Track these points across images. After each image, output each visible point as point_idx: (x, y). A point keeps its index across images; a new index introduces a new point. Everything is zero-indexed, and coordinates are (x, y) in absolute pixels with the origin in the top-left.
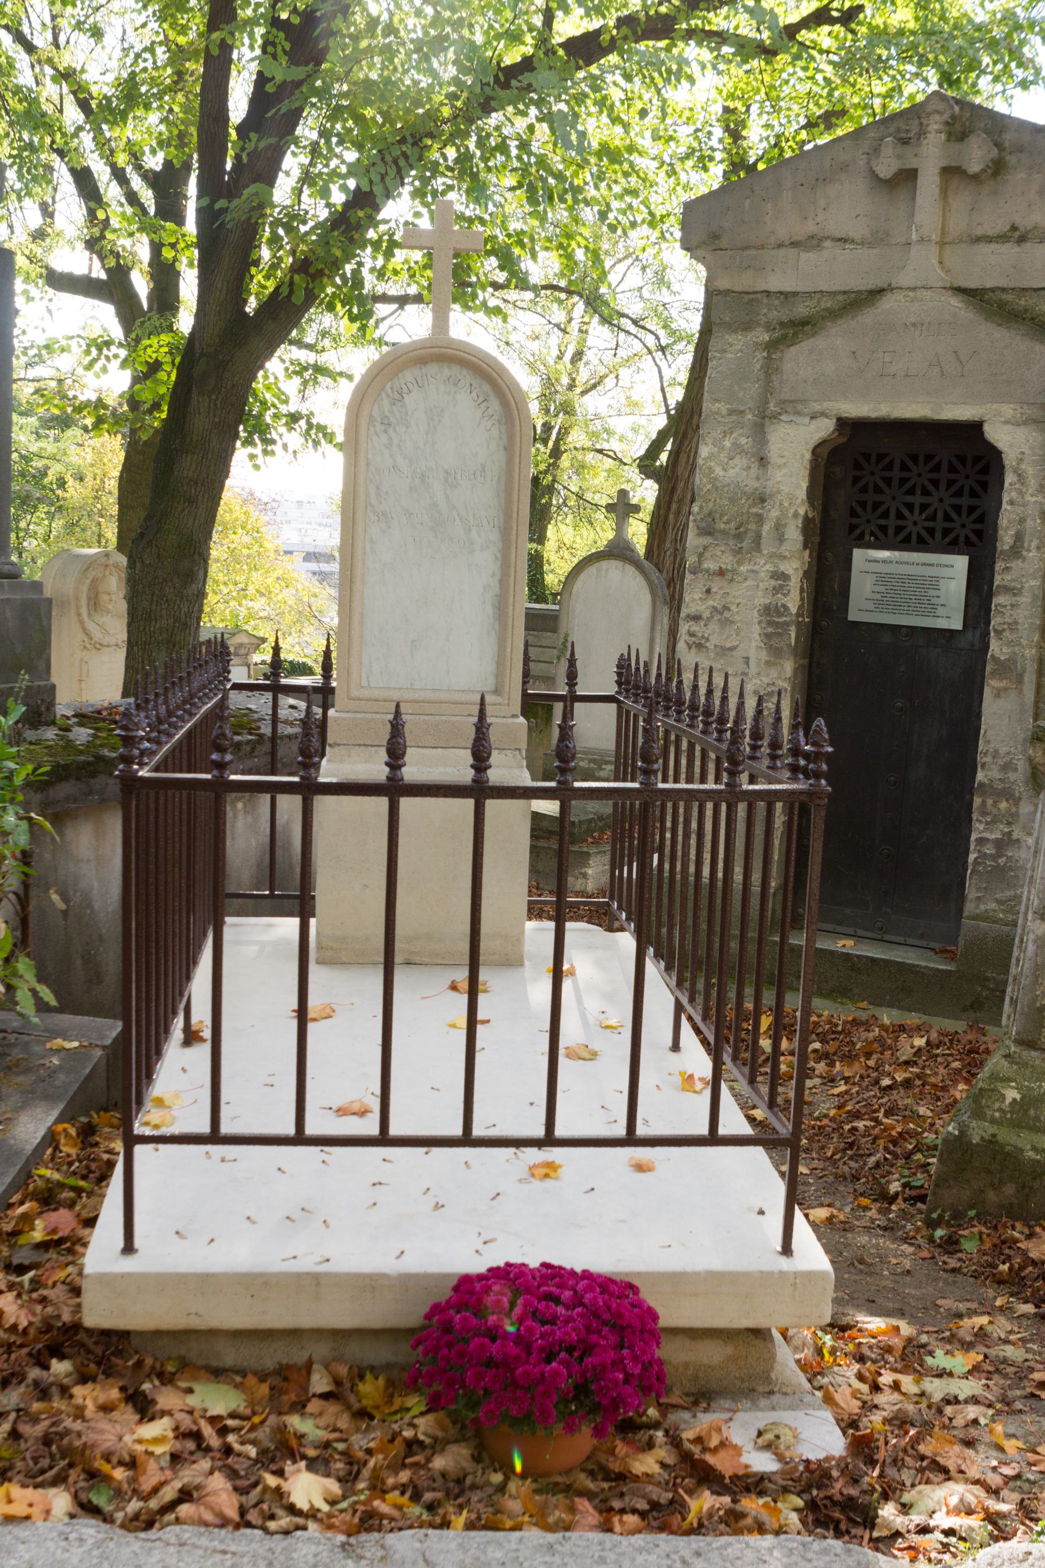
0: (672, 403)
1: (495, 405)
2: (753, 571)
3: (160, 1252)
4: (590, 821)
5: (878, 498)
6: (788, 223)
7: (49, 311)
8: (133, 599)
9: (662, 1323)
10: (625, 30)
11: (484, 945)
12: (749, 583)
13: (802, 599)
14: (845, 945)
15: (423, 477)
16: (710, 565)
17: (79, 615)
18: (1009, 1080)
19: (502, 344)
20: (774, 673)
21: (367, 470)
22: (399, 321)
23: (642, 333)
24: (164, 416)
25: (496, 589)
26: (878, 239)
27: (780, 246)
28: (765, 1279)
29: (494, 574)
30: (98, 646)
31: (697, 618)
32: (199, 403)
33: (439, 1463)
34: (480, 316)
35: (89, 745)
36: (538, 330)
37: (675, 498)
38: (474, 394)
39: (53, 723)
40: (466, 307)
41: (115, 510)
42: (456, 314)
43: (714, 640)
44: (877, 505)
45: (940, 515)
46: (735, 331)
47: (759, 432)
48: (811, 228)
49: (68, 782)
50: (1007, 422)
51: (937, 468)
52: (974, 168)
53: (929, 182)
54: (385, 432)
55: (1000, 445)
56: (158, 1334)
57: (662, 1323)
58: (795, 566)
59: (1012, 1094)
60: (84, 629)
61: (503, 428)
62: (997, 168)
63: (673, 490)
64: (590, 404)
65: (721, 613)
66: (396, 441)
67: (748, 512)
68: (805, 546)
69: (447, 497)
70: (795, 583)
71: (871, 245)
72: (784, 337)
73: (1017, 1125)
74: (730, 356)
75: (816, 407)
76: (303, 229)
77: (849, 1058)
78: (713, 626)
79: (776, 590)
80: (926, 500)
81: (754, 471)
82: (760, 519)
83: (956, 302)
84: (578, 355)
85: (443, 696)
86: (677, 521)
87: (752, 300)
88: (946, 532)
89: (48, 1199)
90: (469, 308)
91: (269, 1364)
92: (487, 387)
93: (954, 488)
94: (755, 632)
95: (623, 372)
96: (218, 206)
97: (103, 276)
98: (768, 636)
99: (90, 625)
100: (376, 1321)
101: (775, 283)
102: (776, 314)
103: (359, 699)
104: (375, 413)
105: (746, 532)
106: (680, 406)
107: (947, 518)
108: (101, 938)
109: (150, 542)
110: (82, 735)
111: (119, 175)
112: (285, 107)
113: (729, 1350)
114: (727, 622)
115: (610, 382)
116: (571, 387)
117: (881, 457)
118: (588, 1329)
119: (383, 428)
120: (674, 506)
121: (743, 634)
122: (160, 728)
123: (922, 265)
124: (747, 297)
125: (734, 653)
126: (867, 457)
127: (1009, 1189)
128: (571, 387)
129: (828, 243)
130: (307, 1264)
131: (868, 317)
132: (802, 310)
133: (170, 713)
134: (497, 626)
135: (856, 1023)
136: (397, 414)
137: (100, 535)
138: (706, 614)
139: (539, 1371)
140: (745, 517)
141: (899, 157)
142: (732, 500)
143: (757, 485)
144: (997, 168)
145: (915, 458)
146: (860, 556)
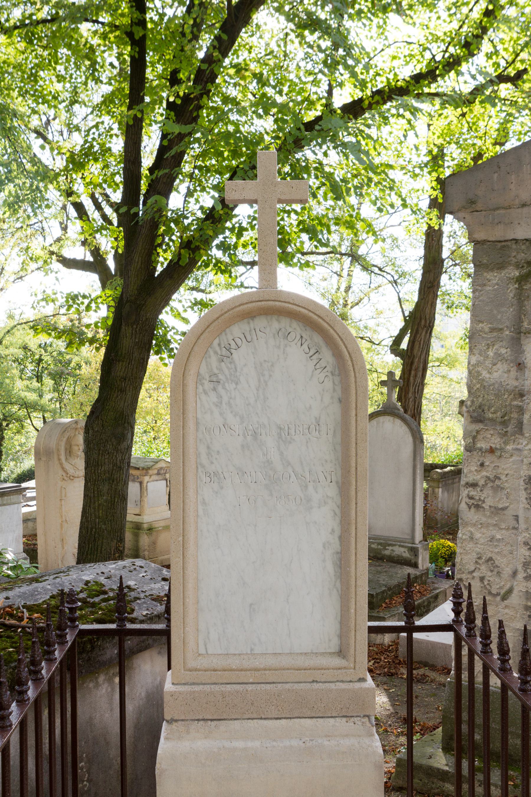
0: (407, 314)
1: (327, 356)
2: (517, 449)
4: (383, 592)
7: (57, 279)
8: (88, 452)
10: (377, 98)
12: (514, 458)
15: (255, 435)
16: (481, 444)
17: (59, 459)
19: (307, 285)
21: (197, 430)
22: (251, 275)
23: (385, 274)
25: (336, 545)
29: (333, 531)
31: (474, 485)
34: (296, 270)
36: (326, 276)
37: (414, 368)
38: (305, 346)
40: (288, 264)
42: (282, 270)
43: (489, 502)
46: (492, 270)
54: (214, 389)
60: (63, 468)
61: (337, 379)
63: (412, 363)
64: (355, 313)
65: (493, 482)
66: (225, 399)
67: (510, 405)
69: (281, 454)
74: (488, 288)
76: (186, 222)
78: (488, 491)
81: (514, 373)
84: (348, 288)
85: (286, 662)
86: (415, 381)
87: (504, 246)
90: (291, 265)
92: (318, 339)
95: (372, 295)
96: (132, 211)
97: (91, 259)
99: (67, 466)
103: (196, 670)
104: (203, 370)
105: (509, 420)
106: (412, 314)
109: (97, 417)
111: (98, 207)
112: (173, 152)
114: (498, 489)
115: (366, 300)
116: (345, 305)
119: (211, 385)
120: (413, 373)
121: (511, 497)
124: (499, 245)
125: (505, 512)
128: (345, 305)
134: (338, 584)
136: (227, 372)
138: (481, 483)
140: (508, 408)
142: (497, 396)
143: (516, 383)
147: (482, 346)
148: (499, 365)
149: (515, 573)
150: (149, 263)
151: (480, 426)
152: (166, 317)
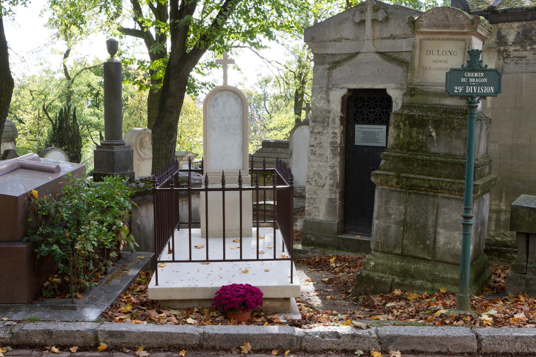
1: (239, 100)
3: (162, 284)
4: (298, 208)
5: (362, 110)
6: (333, 35)
9: (264, 296)
11: (243, 231)
13: (341, 139)
14: (358, 237)
15: (223, 118)
16: (316, 131)
18: (371, 260)
20: (334, 161)
24: (162, 85)
25: (242, 144)
26: (356, 39)
27: (331, 41)
28: (286, 287)
30: (143, 159)
32: (173, 82)
33: (217, 319)
35: (144, 187)
39: (134, 182)
41: (146, 108)
43: (318, 152)
44: (361, 112)
45: (378, 114)
47: (327, 93)
48: (338, 36)
49: (140, 195)
50: (392, 89)
51: (377, 101)
52: (380, 19)
53: (368, 23)
55: (391, 95)
56: (163, 301)
57: (264, 296)
58: (338, 129)
59: (372, 263)
60: (139, 154)
62: (387, 19)
68: (341, 125)
70: (339, 135)
71: (355, 41)
72: (332, 67)
73: (374, 271)
75: (342, 86)
77: (355, 267)
78: (318, 148)
79: (334, 137)
80: (374, 110)
81: (327, 104)
82: (329, 117)
83: (377, 56)
85: (230, 171)
88: (380, 119)
89: (139, 284)
91: (186, 308)
92: (237, 96)
93: (382, 107)
94: (329, 149)
96: (176, 22)
98: (332, 150)
99: (141, 153)
100: (207, 298)
101: (330, 51)
102: (332, 60)
104: (210, 103)
107: (380, 115)
108: (148, 237)
110: (142, 185)
113: (281, 304)
114: (321, 147)
117: (361, 99)
118: (246, 293)
122: (161, 180)
123: (368, 46)
126: (358, 99)
127: (372, 287)
129: (343, 40)
130: (193, 286)
131: (354, 60)
132: (337, 59)
133: (163, 177)
135: (359, 258)
137: (141, 117)
138: (315, 145)
139: (238, 302)
141: (360, 17)
144: (387, 19)
145: (370, 99)
146: (357, 127)
147: (316, 94)
148: (322, 101)
149: (326, 177)
150: (184, 47)
151: (315, 124)
152: (193, 74)
